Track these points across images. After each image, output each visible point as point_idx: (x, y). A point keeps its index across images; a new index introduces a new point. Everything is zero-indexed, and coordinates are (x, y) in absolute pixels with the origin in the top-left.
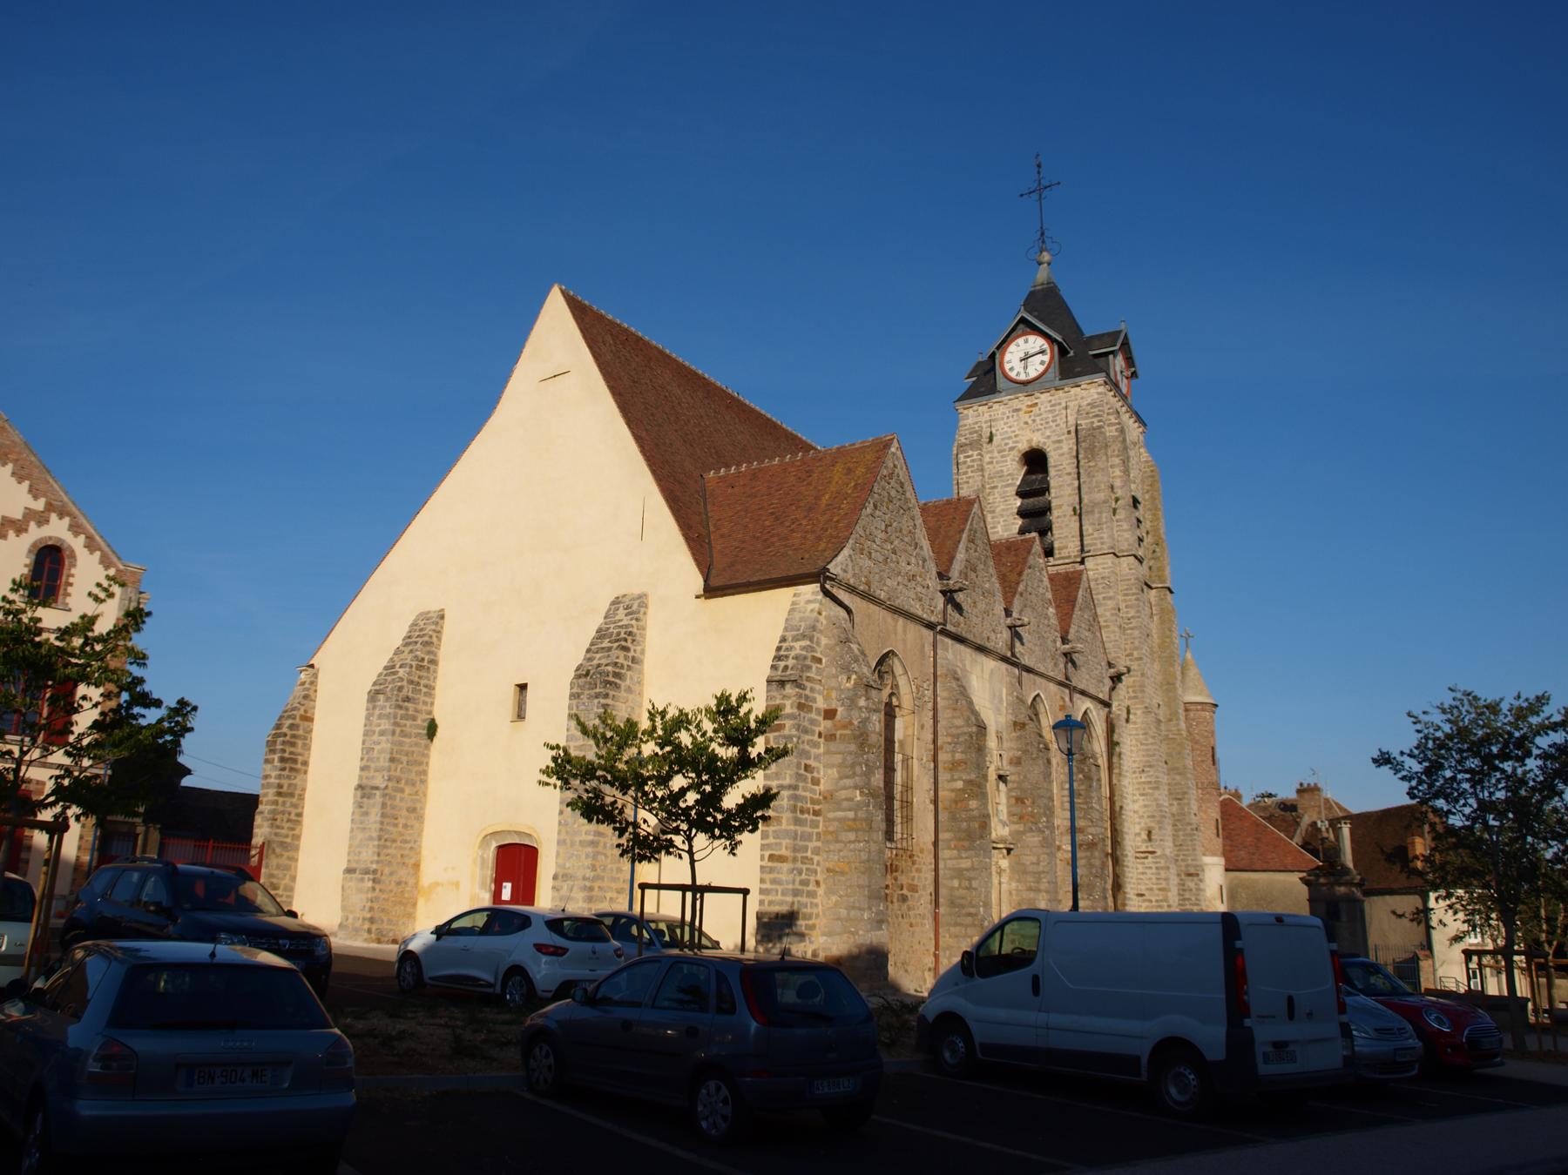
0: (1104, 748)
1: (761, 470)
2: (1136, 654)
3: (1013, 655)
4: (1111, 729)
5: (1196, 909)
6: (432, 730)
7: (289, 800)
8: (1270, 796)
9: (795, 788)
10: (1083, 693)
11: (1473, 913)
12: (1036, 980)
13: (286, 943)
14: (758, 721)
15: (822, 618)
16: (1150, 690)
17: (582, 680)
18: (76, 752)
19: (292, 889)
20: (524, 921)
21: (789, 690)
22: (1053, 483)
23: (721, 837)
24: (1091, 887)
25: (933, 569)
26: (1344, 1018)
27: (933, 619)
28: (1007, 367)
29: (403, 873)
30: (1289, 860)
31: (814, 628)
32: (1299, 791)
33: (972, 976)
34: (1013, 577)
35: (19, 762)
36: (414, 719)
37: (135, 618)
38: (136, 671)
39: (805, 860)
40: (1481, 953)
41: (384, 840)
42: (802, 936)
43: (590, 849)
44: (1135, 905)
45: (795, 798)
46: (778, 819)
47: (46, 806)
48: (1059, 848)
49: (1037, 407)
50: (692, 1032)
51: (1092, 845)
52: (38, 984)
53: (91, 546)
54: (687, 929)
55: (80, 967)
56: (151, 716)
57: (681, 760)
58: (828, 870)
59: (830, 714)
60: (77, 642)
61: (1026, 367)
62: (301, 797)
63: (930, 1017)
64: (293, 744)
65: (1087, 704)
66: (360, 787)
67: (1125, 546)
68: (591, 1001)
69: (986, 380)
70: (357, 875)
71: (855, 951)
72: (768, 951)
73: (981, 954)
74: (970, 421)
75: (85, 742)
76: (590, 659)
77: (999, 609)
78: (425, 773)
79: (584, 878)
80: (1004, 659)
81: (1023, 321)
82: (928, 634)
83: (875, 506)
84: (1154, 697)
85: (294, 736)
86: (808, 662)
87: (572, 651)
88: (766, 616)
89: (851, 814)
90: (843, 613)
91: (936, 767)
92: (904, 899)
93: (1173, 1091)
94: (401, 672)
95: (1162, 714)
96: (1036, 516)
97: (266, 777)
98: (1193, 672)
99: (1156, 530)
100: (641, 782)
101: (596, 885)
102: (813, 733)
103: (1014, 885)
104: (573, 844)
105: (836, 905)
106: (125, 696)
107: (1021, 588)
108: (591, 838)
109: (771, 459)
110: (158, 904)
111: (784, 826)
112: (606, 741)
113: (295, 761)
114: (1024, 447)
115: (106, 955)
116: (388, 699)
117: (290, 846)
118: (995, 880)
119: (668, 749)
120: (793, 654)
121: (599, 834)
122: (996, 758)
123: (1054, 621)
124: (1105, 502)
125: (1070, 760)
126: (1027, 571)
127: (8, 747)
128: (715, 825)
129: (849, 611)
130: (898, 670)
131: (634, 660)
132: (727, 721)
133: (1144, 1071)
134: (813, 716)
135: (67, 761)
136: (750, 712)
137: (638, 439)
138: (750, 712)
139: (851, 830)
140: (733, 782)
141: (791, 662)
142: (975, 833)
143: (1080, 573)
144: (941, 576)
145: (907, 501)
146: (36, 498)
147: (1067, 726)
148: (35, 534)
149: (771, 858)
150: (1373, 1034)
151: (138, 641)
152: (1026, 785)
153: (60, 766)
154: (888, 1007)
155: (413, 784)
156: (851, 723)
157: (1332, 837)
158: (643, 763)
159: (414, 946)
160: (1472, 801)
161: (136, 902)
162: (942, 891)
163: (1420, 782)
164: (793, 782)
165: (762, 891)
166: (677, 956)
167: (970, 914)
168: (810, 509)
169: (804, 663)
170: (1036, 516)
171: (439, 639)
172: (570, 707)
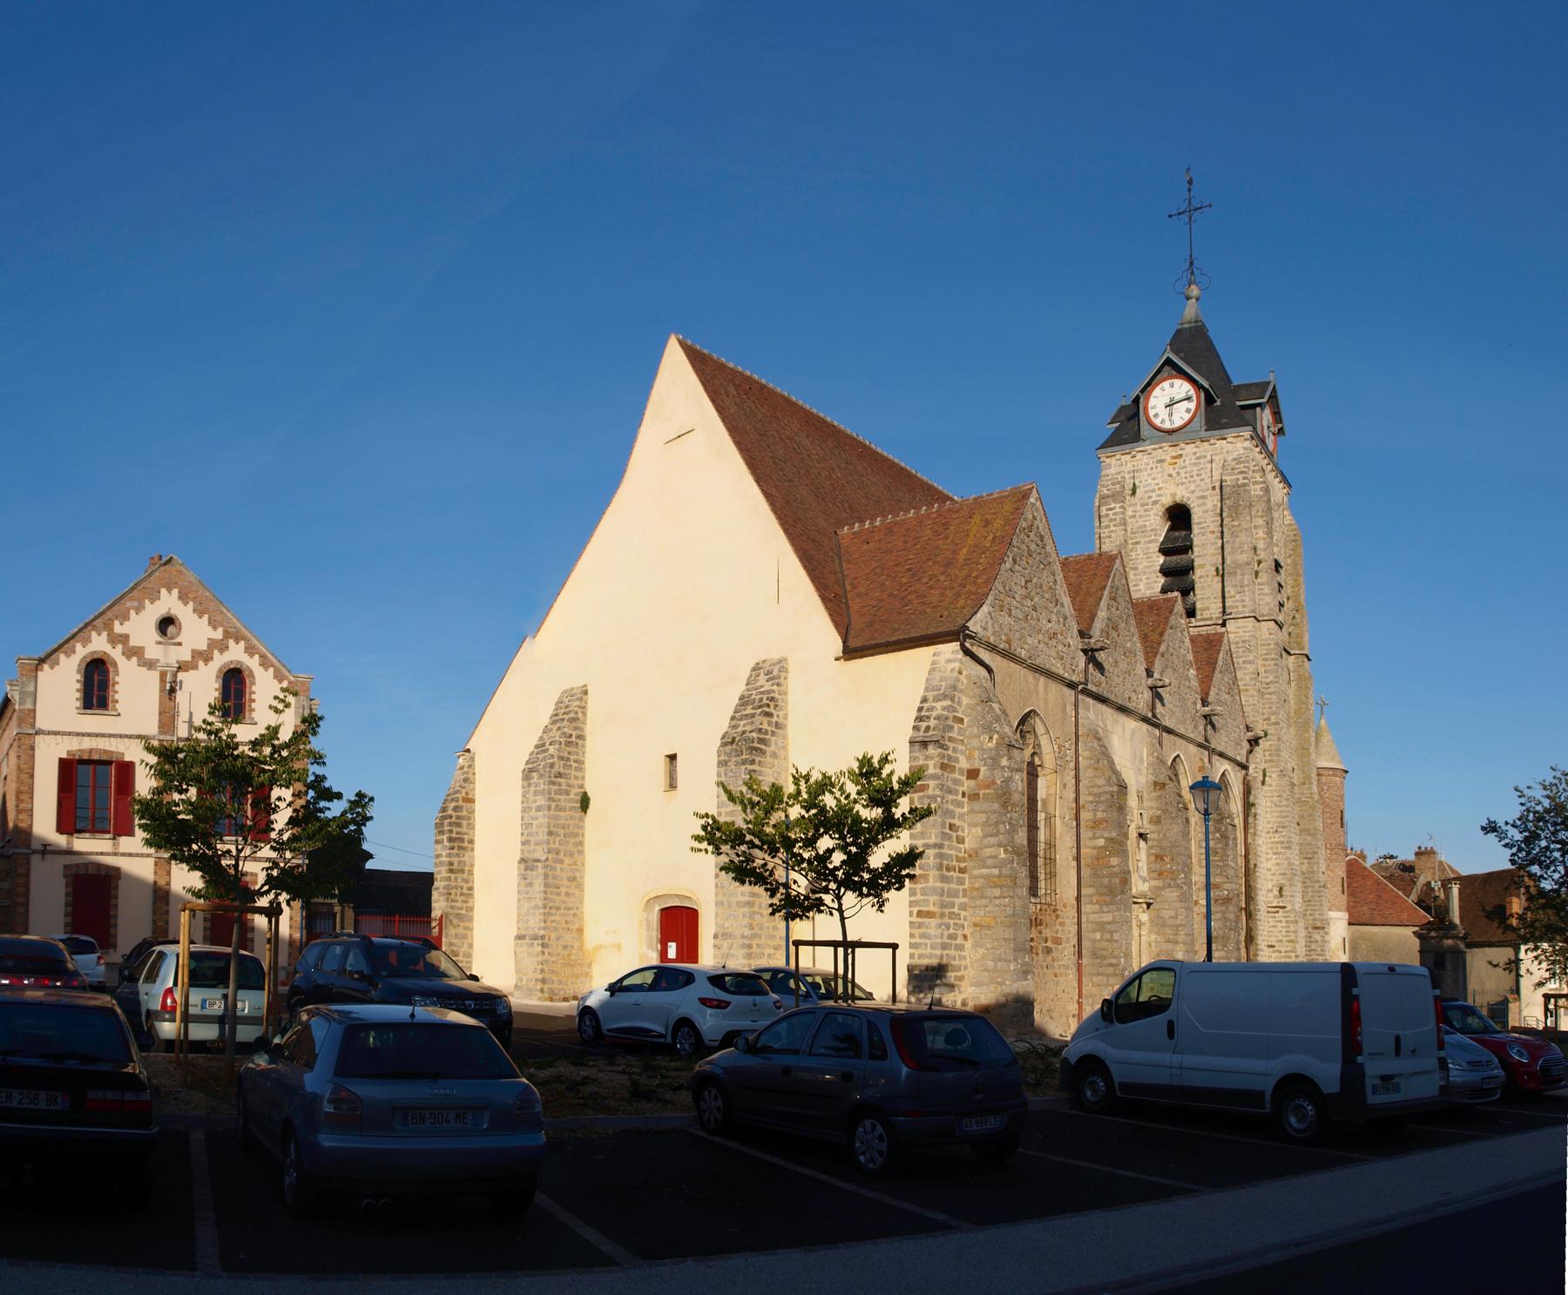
0: (1240, 809)
1: (895, 523)
2: (1273, 719)
3: (1154, 715)
4: (1247, 790)
5: (1321, 959)
6: (585, 802)
7: (459, 876)
8: (1392, 857)
9: (941, 846)
10: (1221, 755)
11: (1554, 962)
12: (1171, 1025)
13: (471, 1004)
14: (900, 782)
15: (962, 678)
16: (1285, 754)
17: (729, 748)
18: (280, 847)
19: (470, 956)
20: (689, 978)
21: (932, 750)
22: (1196, 542)
23: (868, 895)
24: (1225, 939)
25: (1074, 628)
26: (1442, 1054)
27: (1074, 678)
28: (1152, 413)
29: (568, 938)
30: (1405, 916)
31: (954, 688)
32: (1417, 854)
33: (1111, 1022)
34: (1155, 637)
35: (237, 859)
36: (567, 793)
37: (311, 722)
38: (319, 770)
39: (952, 915)
40: (1557, 997)
41: (548, 908)
42: (951, 987)
43: (746, 910)
44: (1265, 956)
45: (941, 856)
46: (925, 877)
47: (262, 894)
48: (1196, 903)
49: (1180, 464)
50: (847, 1077)
51: (1227, 900)
52: (277, 1040)
53: (265, 664)
54: (840, 982)
55: (307, 1027)
56: (335, 809)
57: (824, 822)
58: (975, 925)
59: (973, 774)
60: (267, 751)
61: (1171, 415)
62: (471, 873)
63: (1073, 1060)
64: (459, 825)
65: (1225, 766)
66: (523, 860)
67: (1266, 611)
68: (752, 1049)
69: (1129, 426)
70: (527, 941)
71: (1003, 999)
72: (919, 1000)
73: (1121, 1001)
74: (1112, 471)
75: (285, 837)
76: (735, 727)
77: (1141, 669)
78: (581, 844)
79: (743, 937)
80: (1145, 720)
81: (1169, 362)
82: (1070, 693)
83: (1014, 561)
84: (1289, 761)
85: (458, 817)
86: (950, 722)
87: (718, 721)
88: (906, 678)
89: (996, 871)
90: (984, 672)
91: (1078, 825)
92: (1048, 951)
93: (1293, 1120)
94: (552, 750)
95: (1296, 777)
96: (1179, 575)
97: (438, 856)
98: (1326, 739)
99: (1297, 596)
100: (789, 844)
101: (754, 942)
102: (956, 792)
103: (1153, 937)
104: (730, 905)
105: (983, 956)
106: (311, 793)
107: (1162, 648)
108: (746, 898)
109: (907, 511)
110: (360, 973)
111: (931, 883)
112: (753, 805)
113: (462, 840)
114: (1167, 501)
115: (326, 1017)
116: (541, 776)
117: (466, 917)
118: (1135, 933)
119: (813, 811)
120: (934, 714)
121: (754, 895)
122: (1136, 817)
123: (1195, 683)
124: (1248, 564)
125: (1206, 820)
126: (1169, 631)
127: (227, 847)
128: (862, 883)
129: (990, 671)
130: (1040, 729)
131: (777, 725)
132: (869, 782)
133: (1268, 1106)
134: (956, 776)
135: (274, 855)
136: (892, 773)
137: (768, 496)
138: (892, 773)
139: (996, 886)
140: (877, 843)
141: (932, 723)
142: (1117, 889)
143: (1221, 635)
144: (1083, 634)
145: (1047, 555)
146: (215, 628)
147: (1204, 787)
148: (220, 661)
149: (920, 914)
150: (1466, 1066)
151: (316, 743)
152: (1165, 843)
153: (268, 860)
154: (1033, 1051)
155: (572, 855)
156: (994, 783)
157: (1442, 896)
158: (788, 826)
159: (592, 1002)
160: (1561, 868)
161: (342, 971)
162: (1085, 944)
163: (1520, 850)
164: (939, 841)
165: (912, 946)
166: (832, 1008)
167: (1111, 965)
168: (948, 564)
169: (945, 723)
170: (1179, 575)
171: (584, 714)
172: (719, 775)
